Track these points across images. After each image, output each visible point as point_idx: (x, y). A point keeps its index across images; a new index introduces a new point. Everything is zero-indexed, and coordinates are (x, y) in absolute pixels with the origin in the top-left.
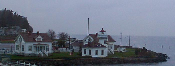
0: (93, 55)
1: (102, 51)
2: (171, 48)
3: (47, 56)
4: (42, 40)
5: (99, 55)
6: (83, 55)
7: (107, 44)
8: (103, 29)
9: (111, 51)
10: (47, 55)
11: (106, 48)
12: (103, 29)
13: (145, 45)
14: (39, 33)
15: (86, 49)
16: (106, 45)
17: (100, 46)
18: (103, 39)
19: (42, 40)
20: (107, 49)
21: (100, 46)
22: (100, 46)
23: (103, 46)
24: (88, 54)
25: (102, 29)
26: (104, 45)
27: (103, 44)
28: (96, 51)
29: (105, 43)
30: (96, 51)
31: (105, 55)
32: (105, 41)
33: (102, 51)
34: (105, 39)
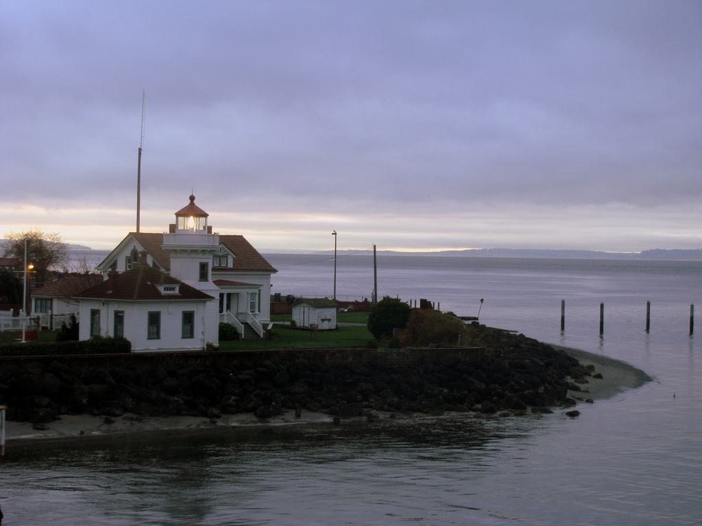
0: (140, 342)
1: (188, 318)
2: (261, 309)
3: (262, 336)
4: (230, 265)
5: (172, 340)
6: (84, 335)
7: (217, 283)
8: (192, 198)
9: (249, 322)
10: (261, 333)
11: (209, 304)
12: (192, 198)
13: (482, 300)
14: (214, 231)
15: (96, 306)
16: (208, 287)
17: (177, 291)
18: (193, 255)
19: (230, 265)
20: (213, 306)
21: (173, 289)
22: (173, 289)
23: (189, 294)
24: (107, 329)
25: (189, 202)
26: (198, 288)
27: (193, 282)
28: (154, 319)
29: (203, 277)
30: (154, 319)
31: (206, 334)
32: (203, 267)
33: (188, 318)
34: (204, 252)
